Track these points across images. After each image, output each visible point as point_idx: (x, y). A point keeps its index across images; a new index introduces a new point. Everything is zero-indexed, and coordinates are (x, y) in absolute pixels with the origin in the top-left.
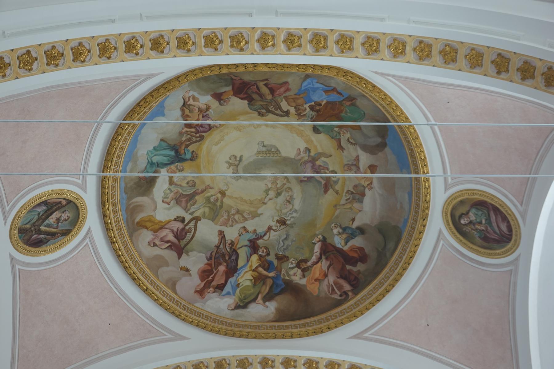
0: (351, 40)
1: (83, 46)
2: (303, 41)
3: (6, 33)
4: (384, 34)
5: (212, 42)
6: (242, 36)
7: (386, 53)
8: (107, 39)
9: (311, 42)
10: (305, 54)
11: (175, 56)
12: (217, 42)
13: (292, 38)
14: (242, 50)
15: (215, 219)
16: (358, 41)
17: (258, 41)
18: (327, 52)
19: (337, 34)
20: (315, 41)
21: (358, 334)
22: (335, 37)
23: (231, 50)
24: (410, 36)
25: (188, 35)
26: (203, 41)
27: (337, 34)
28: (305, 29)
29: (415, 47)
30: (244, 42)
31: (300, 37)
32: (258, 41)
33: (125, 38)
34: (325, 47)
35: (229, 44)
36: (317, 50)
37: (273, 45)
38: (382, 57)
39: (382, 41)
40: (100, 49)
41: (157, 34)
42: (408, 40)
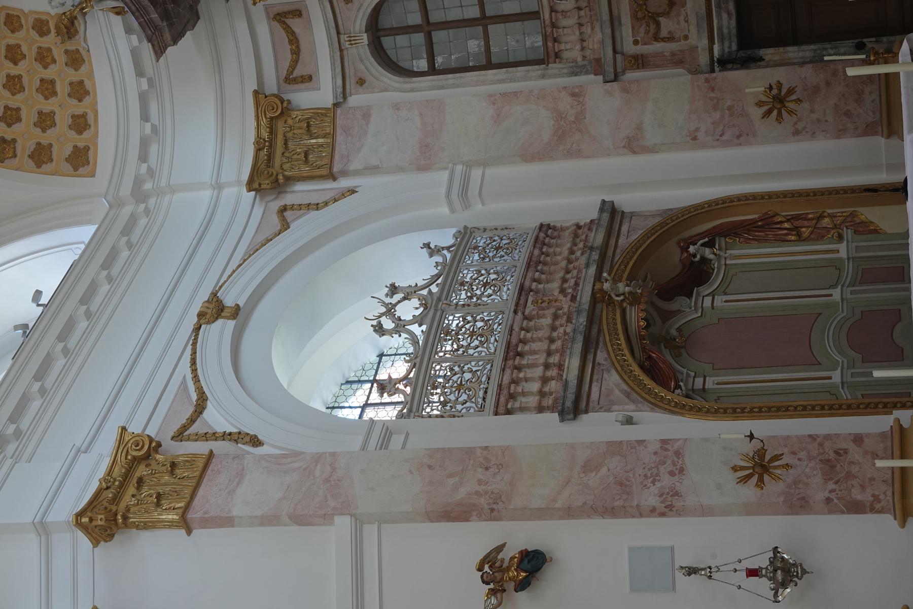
3: (296, 24)
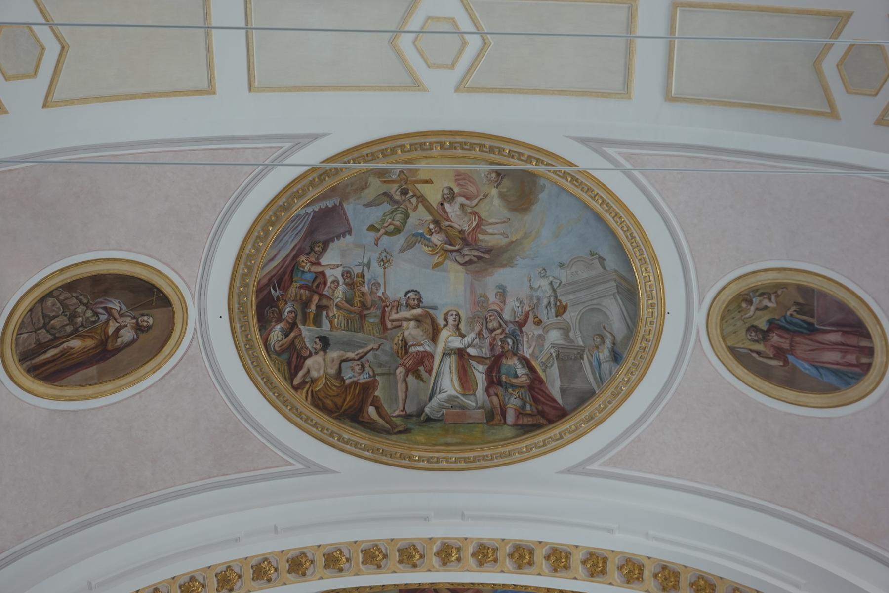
0: (568, 555)
1: (196, 580)
2: (500, 555)
3: (93, 584)
4: (613, 551)
5: (374, 557)
6: (416, 549)
7: (616, 576)
8: (229, 567)
9: (511, 556)
10: (502, 572)
11: (321, 578)
12: (381, 557)
13: (485, 551)
14: (415, 566)
15: (363, 327)
16: (577, 558)
17: (437, 554)
18: (534, 569)
19: (548, 547)
20: (516, 555)
21: (579, 465)
22: (544, 551)
23: (400, 567)
24: (649, 558)
25: (340, 550)
26: (361, 556)
27: (548, 547)
28: (503, 540)
29: (656, 572)
30: (418, 557)
31: (495, 550)
32: (437, 554)
33: (254, 563)
34: (531, 563)
35: (397, 559)
36: (520, 567)
37: (459, 560)
38: (611, 581)
39: (610, 560)
40: (218, 580)
41: (297, 552)
42: (646, 562)
